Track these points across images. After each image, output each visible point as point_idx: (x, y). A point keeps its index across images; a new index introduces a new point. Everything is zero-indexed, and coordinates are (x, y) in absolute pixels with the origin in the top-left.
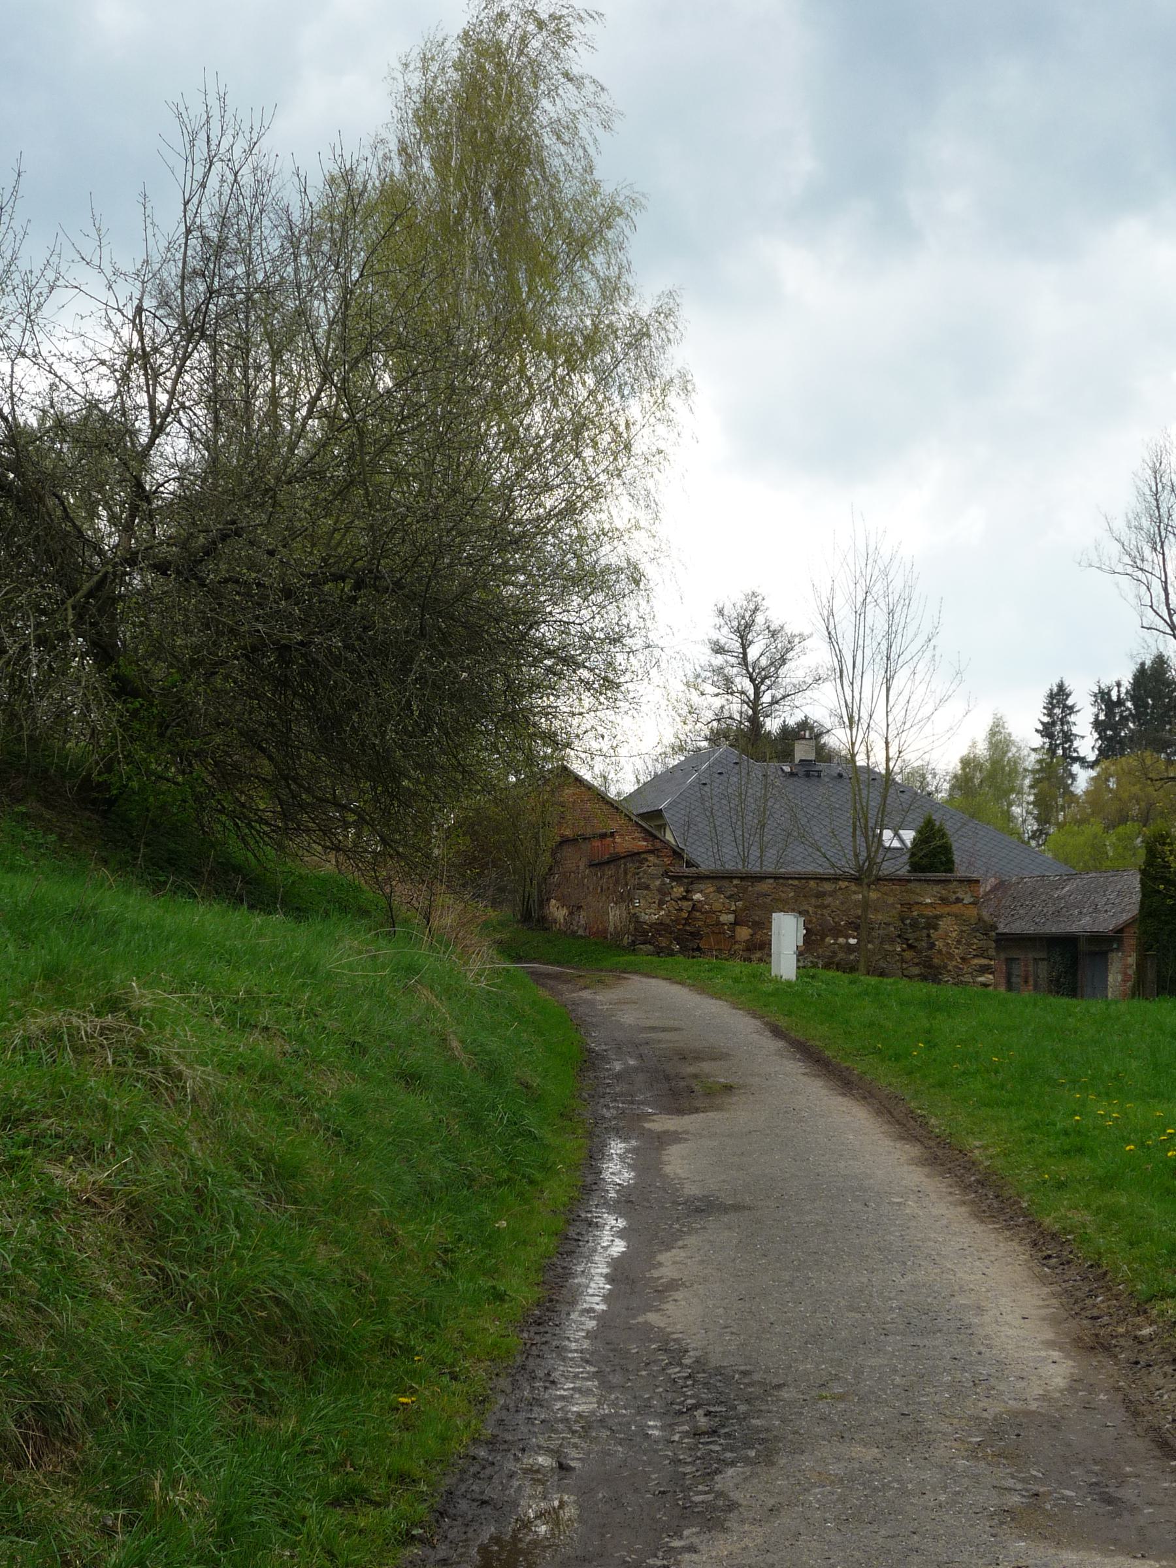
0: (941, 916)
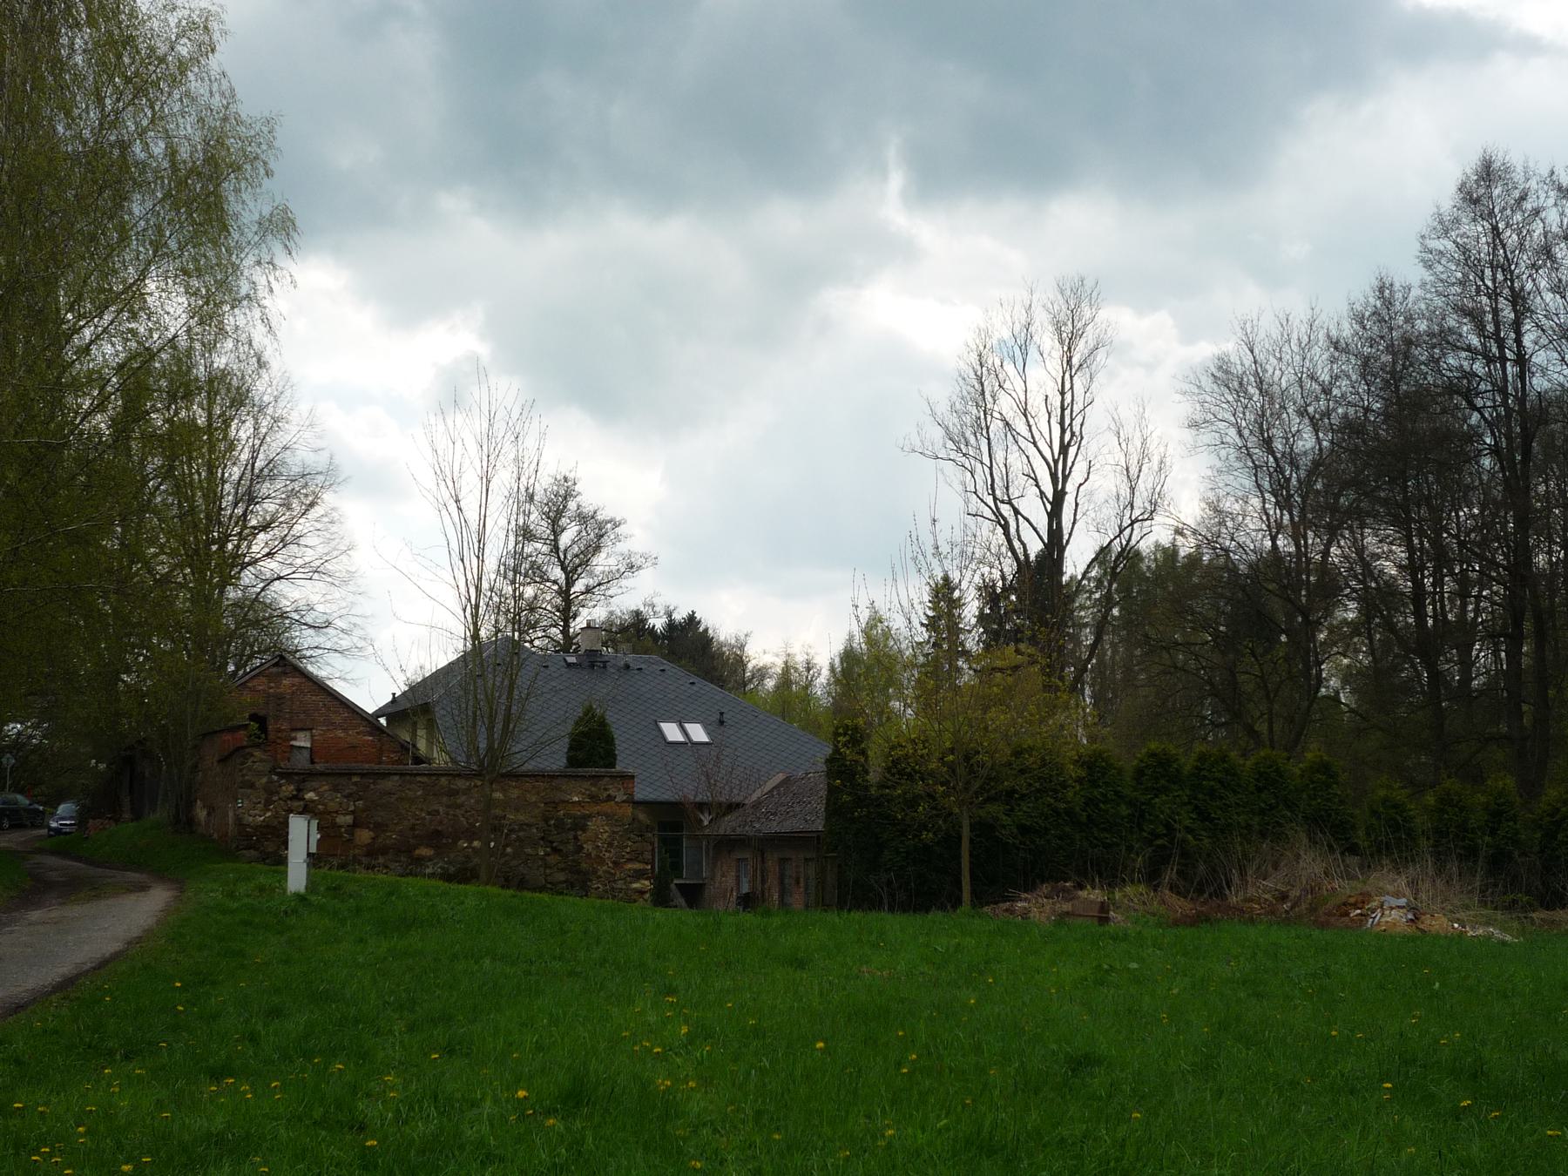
0: (590, 816)
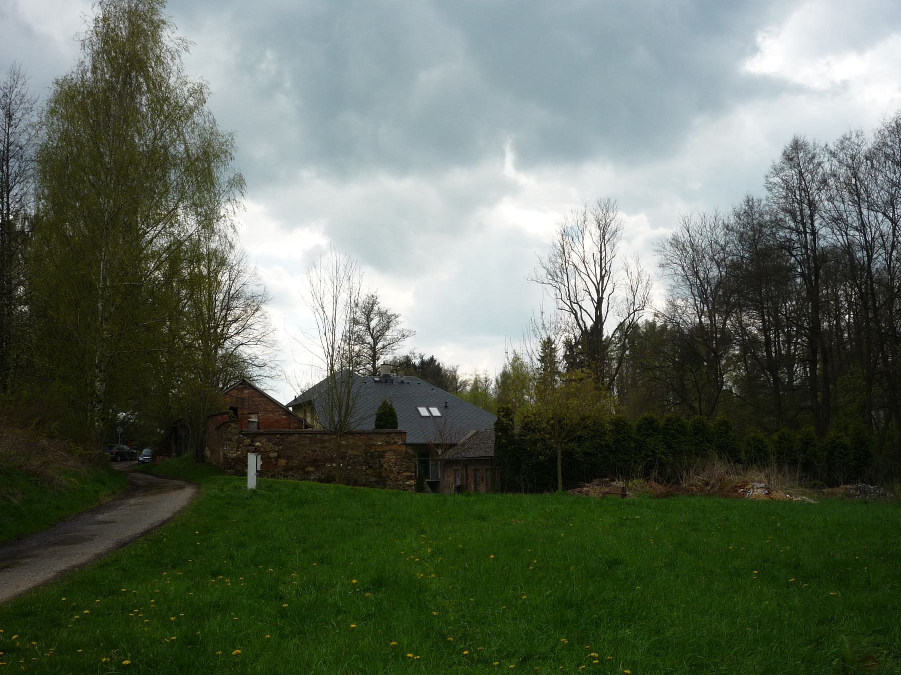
0: (386, 451)
